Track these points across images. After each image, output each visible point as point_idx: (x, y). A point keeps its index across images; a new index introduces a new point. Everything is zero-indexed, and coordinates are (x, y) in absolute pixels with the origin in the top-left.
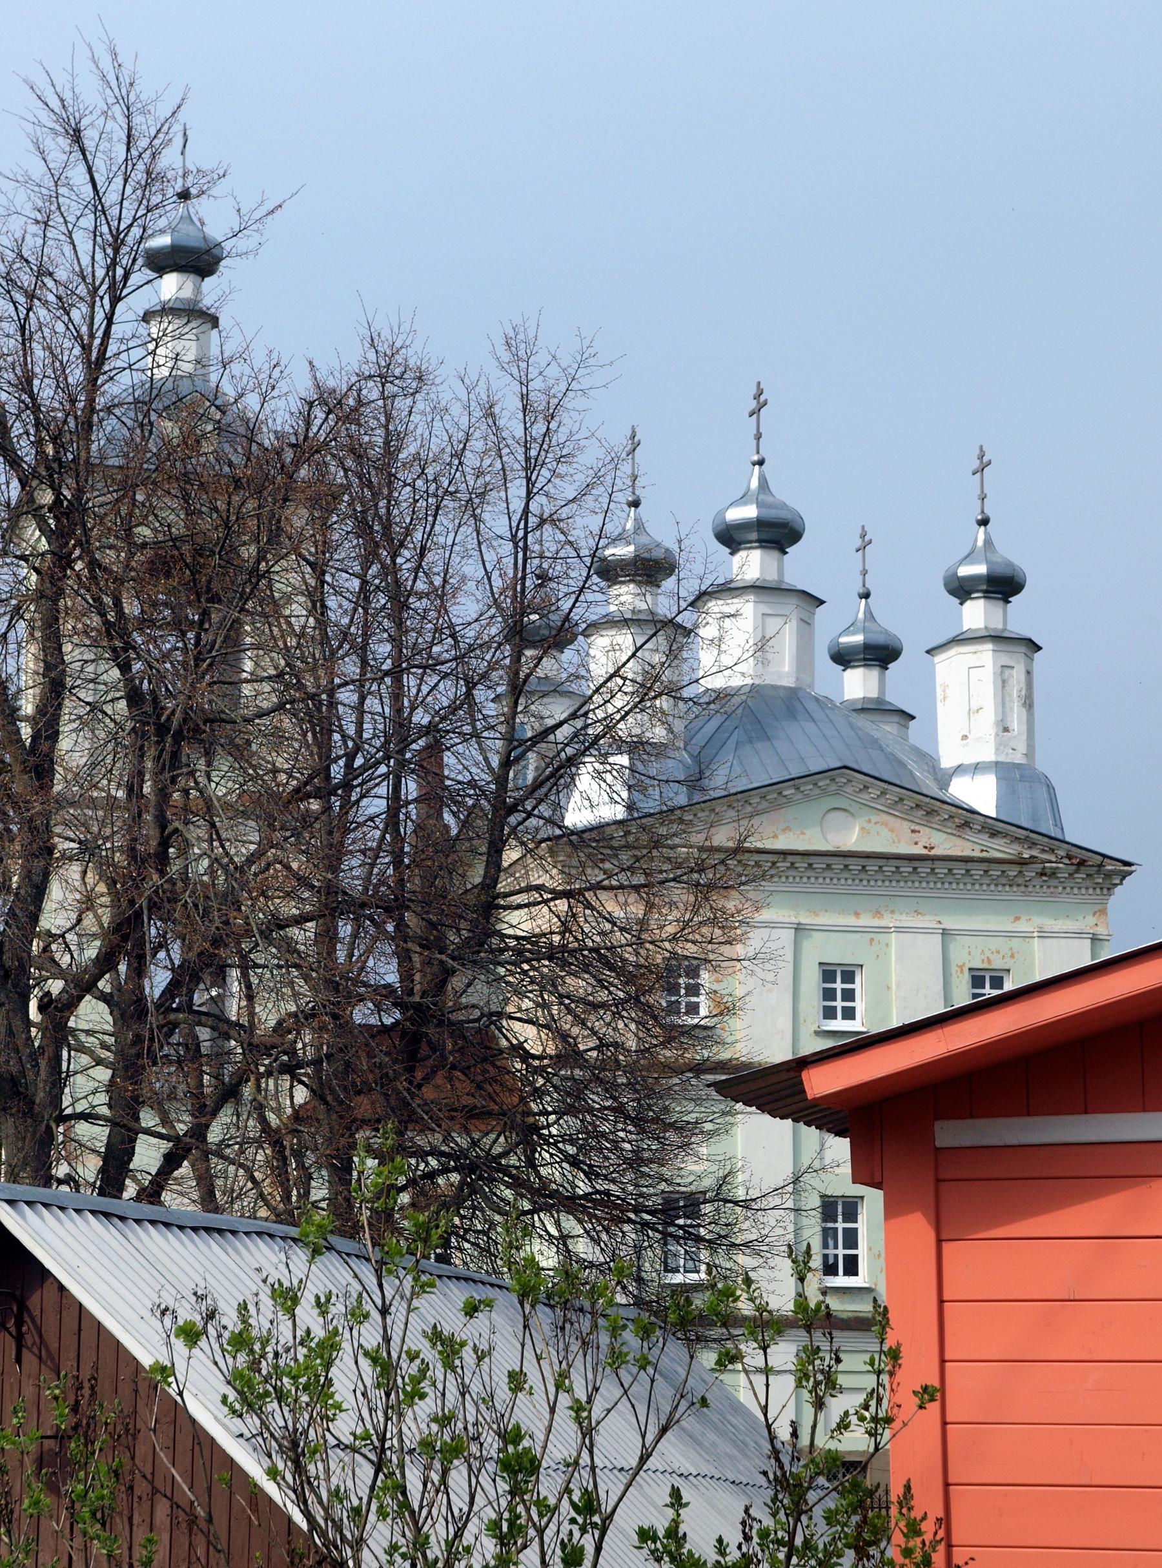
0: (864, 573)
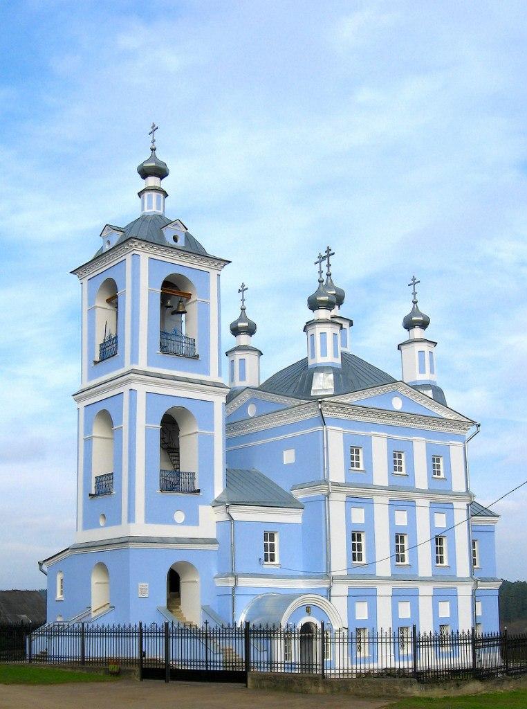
0: (243, 300)
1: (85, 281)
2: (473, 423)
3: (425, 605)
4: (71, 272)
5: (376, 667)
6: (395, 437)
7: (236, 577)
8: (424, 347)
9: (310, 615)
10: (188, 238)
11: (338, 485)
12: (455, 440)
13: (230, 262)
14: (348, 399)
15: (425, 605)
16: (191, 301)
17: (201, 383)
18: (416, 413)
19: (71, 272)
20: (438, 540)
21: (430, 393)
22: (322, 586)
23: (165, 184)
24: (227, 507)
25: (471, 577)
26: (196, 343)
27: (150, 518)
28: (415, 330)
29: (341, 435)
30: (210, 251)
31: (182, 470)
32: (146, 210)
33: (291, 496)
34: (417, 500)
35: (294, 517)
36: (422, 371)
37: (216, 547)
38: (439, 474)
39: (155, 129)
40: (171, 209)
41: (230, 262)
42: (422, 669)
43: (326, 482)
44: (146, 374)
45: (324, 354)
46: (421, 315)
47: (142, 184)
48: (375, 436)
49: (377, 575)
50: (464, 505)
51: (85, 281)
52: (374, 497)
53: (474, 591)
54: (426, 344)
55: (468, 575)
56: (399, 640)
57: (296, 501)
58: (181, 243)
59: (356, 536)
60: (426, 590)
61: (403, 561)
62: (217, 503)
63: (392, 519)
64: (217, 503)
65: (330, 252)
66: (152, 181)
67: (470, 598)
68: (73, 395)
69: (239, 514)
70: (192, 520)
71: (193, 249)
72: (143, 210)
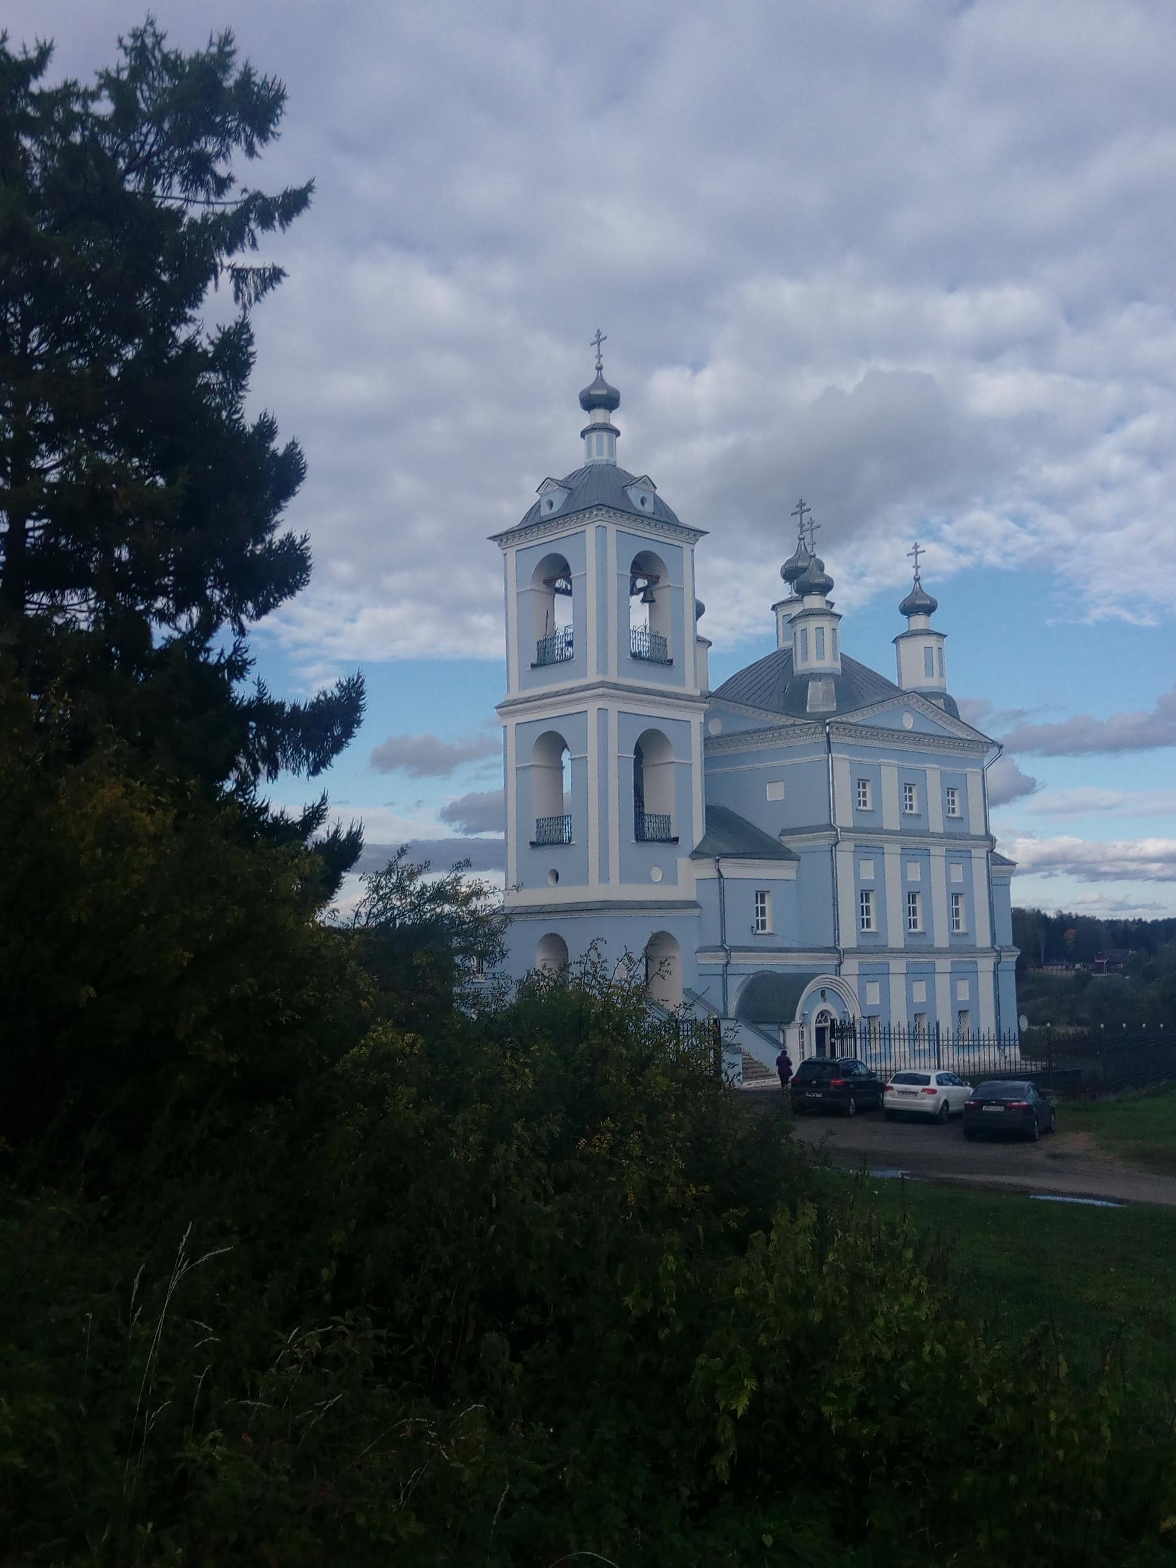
1: (511, 552)
2: (994, 743)
3: (942, 983)
4: (493, 538)
5: (893, 1067)
6: (907, 765)
7: (728, 951)
8: (932, 641)
9: (825, 1000)
10: (658, 502)
11: (847, 830)
12: (973, 767)
13: (704, 533)
14: (854, 718)
15: (897, 984)
16: (658, 586)
17: (677, 696)
18: (923, 731)
19: (493, 538)
20: (912, 897)
21: (941, 703)
22: (714, 961)
23: (617, 420)
24: (718, 861)
25: (992, 947)
26: (668, 643)
27: (624, 878)
28: (917, 617)
29: (847, 764)
30: (683, 519)
31: (646, 812)
32: (595, 457)
33: (780, 844)
34: (885, 846)
35: (783, 871)
36: (929, 673)
37: (696, 912)
38: (911, 808)
39: (599, 339)
40: (629, 454)
41: (704, 533)
42: (961, 1068)
43: (830, 827)
44: (616, 687)
45: (821, 655)
46: (928, 597)
47: (586, 419)
48: (885, 764)
49: (936, 946)
50: (982, 853)
51: (511, 552)
52: (885, 846)
53: (996, 965)
54: (935, 638)
55: (989, 944)
56: (914, 1036)
57: (789, 851)
58: (649, 508)
59: (865, 896)
60: (898, 965)
61: (915, 927)
62: (696, 854)
63: (904, 874)
64: (696, 854)
65: (804, 508)
66: (599, 416)
67: (991, 975)
68: (497, 708)
69: (732, 869)
70: (671, 878)
71: (664, 518)
72: (589, 454)
